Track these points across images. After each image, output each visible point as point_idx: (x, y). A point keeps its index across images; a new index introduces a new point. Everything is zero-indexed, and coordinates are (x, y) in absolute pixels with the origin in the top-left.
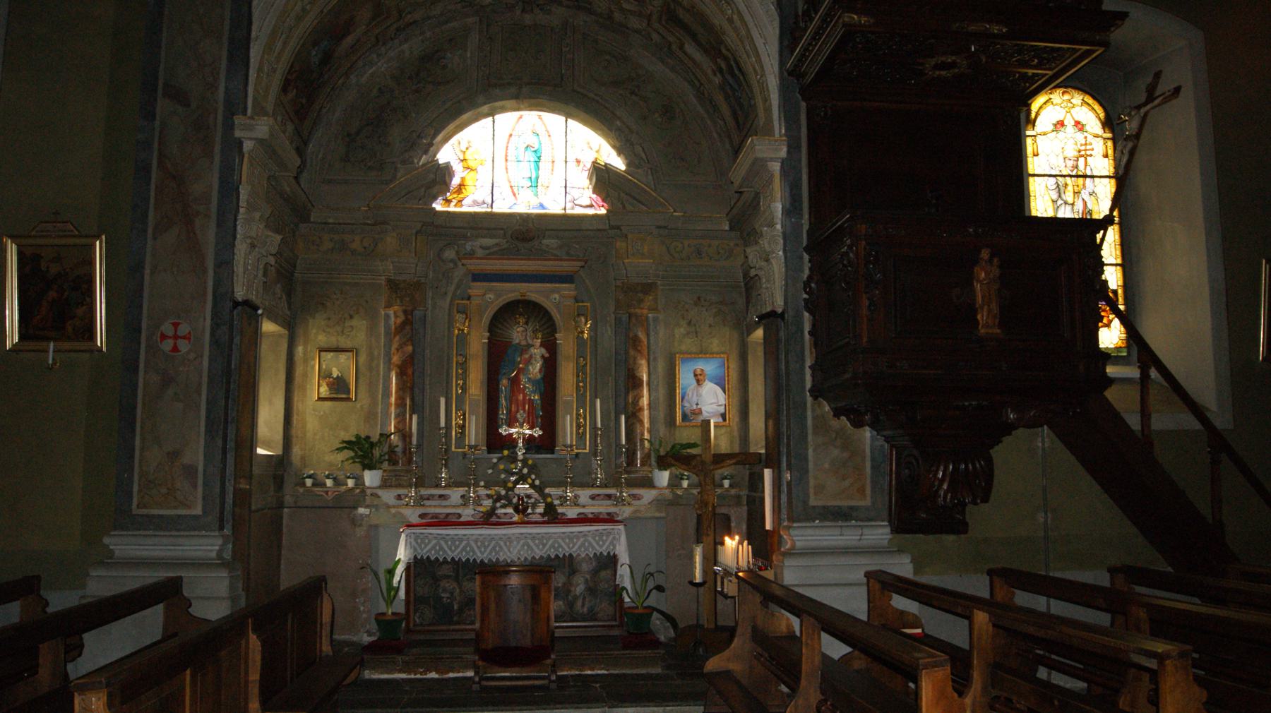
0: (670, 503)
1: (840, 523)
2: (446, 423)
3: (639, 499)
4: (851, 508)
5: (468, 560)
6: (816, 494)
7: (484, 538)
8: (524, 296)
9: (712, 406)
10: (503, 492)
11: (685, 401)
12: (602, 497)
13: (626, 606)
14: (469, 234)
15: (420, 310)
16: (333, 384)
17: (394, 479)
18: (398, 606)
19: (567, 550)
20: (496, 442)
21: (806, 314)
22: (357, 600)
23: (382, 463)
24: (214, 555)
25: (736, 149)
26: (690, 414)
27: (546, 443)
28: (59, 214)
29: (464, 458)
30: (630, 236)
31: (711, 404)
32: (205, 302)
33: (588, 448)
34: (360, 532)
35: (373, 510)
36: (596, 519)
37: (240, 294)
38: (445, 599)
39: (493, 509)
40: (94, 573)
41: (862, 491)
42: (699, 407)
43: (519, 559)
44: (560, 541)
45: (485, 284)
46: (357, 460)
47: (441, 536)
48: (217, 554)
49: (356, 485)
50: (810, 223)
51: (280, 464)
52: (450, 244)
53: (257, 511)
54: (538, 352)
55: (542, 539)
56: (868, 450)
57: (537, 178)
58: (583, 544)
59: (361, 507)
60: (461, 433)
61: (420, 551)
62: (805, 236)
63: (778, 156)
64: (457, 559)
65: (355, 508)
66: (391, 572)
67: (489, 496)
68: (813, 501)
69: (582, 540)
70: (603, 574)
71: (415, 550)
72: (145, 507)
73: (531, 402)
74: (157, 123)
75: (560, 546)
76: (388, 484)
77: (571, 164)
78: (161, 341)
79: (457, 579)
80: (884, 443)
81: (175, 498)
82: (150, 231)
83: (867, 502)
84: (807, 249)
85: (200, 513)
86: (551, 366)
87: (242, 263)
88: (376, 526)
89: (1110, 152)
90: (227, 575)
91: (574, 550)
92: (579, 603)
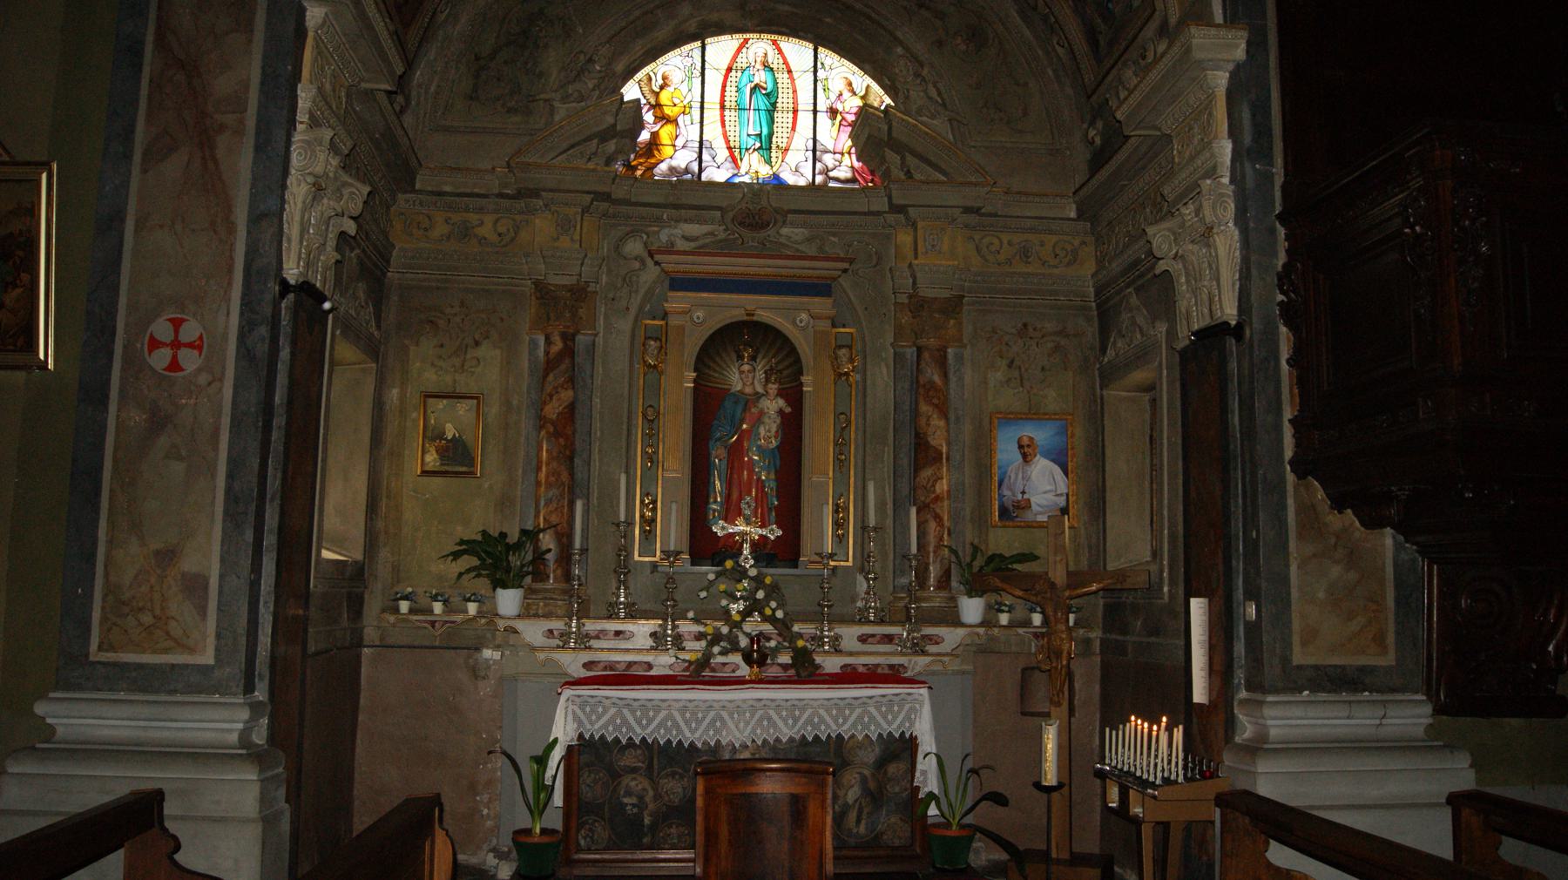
0: (982, 650)
1: (1344, 696)
2: (627, 516)
3: (937, 643)
4: (1363, 670)
5: (669, 741)
6: (1304, 644)
7: (696, 707)
8: (753, 315)
9: (1046, 496)
10: (725, 630)
11: (1004, 487)
12: (878, 638)
13: (930, 821)
14: (665, 217)
15: (584, 334)
16: (446, 449)
17: (541, 604)
18: (553, 818)
19: (834, 727)
20: (705, 547)
21: (1283, 329)
22: (478, 798)
23: (523, 577)
24: (234, 738)
25: (1090, 93)
26: (1011, 508)
27: (782, 552)
29: (652, 572)
30: (920, 224)
31: (1045, 493)
32: (230, 284)
33: (851, 559)
34: (485, 688)
35: (507, 653)
36: (871, 677)
37: (292, 272)
38: (629, 808)
39: (707, 656)
40: (14, 768)
41: (1379, 639)
42: (1026, 496)
43: (753, 741)
44: (822, 712)
45: (689, 294)
46: (484, 572)
47: (624, 702)
48: (240, 738)
49: (478, 612)
50: (1286, 175)
51: (354, 578)
52: (632, 232)
53: (317, 654)
54: (773, 405)
55: (795, 707)
56: (1389, 570)
57: (771, 135)
58: (860, 718)
59: (488, 648)
60: (650, 531)
61: (589, 727)
62: (1278, 194)
63: (1230, 58)
64: (650, 741)
65: (478, 649)
66: (541, 761)
67: (699, 637)
68: (1298, 657)
69: (858, 711)
70: (892, 769)
71: (580, 723)
72: (112, 648)
73: (761, 485)
75: (822, 721)
76: (532, 612)
77: (823, 119)
78: (150, 352)
79: (650, 772)
80: (1417, 555)
81: (168, 633)
82: (137, 157)
83: (1389, 660)
84: (1281, 218)
85: (211, 662)
86: (792, 426)
87: (297, 218)
88: (514, 679)
90: (255, 778)
91: (845, 727)
92: (853, 815)
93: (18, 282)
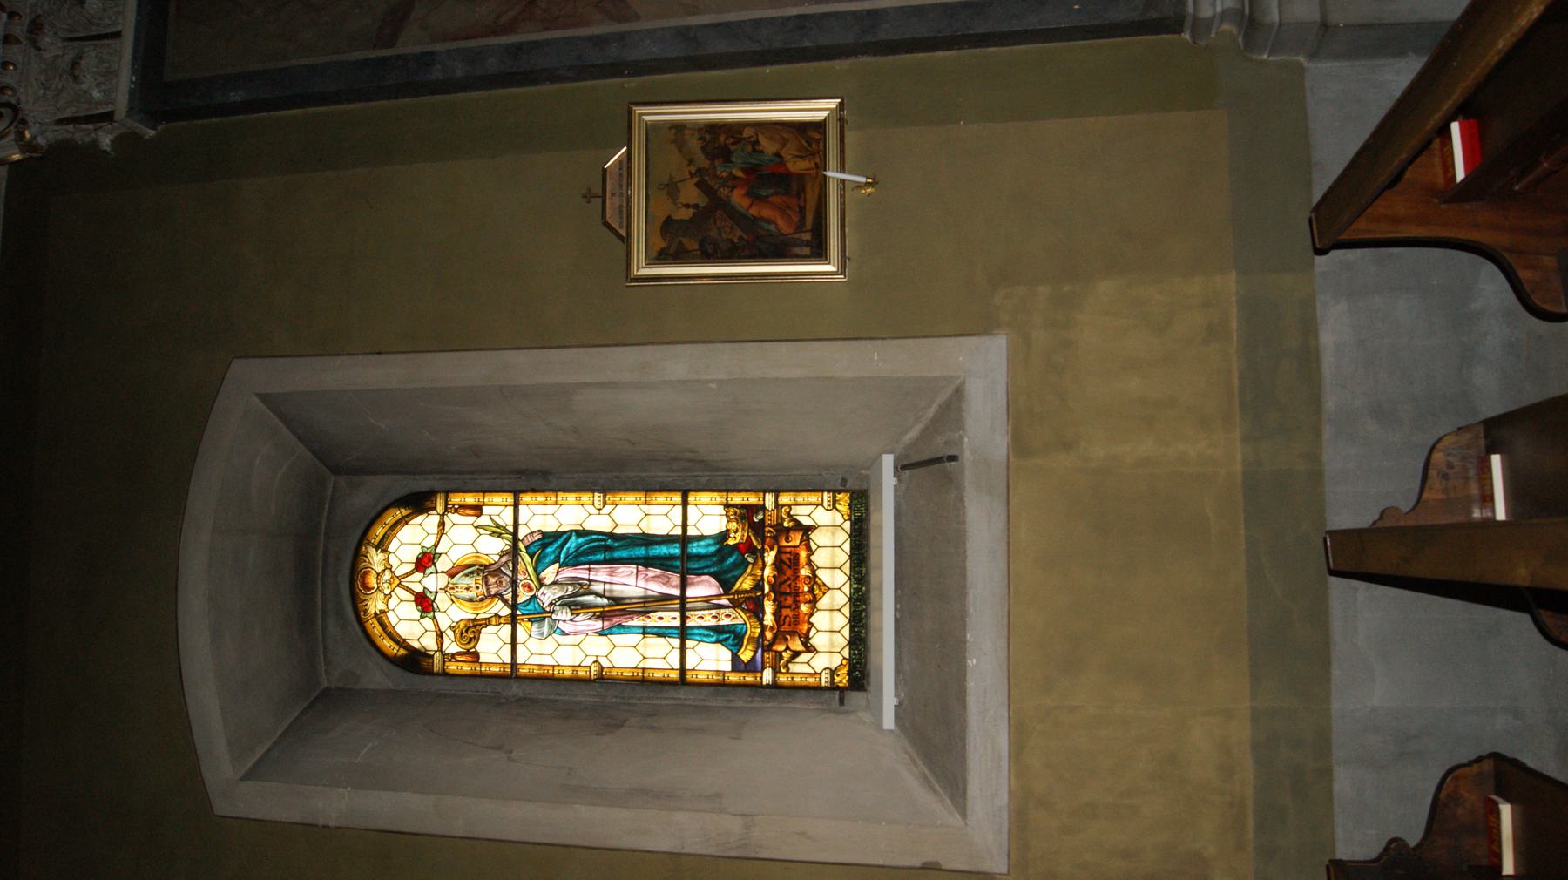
28: (584, 196)
74: (438, 47)
89: (470, 499)
93: (752, 139)
